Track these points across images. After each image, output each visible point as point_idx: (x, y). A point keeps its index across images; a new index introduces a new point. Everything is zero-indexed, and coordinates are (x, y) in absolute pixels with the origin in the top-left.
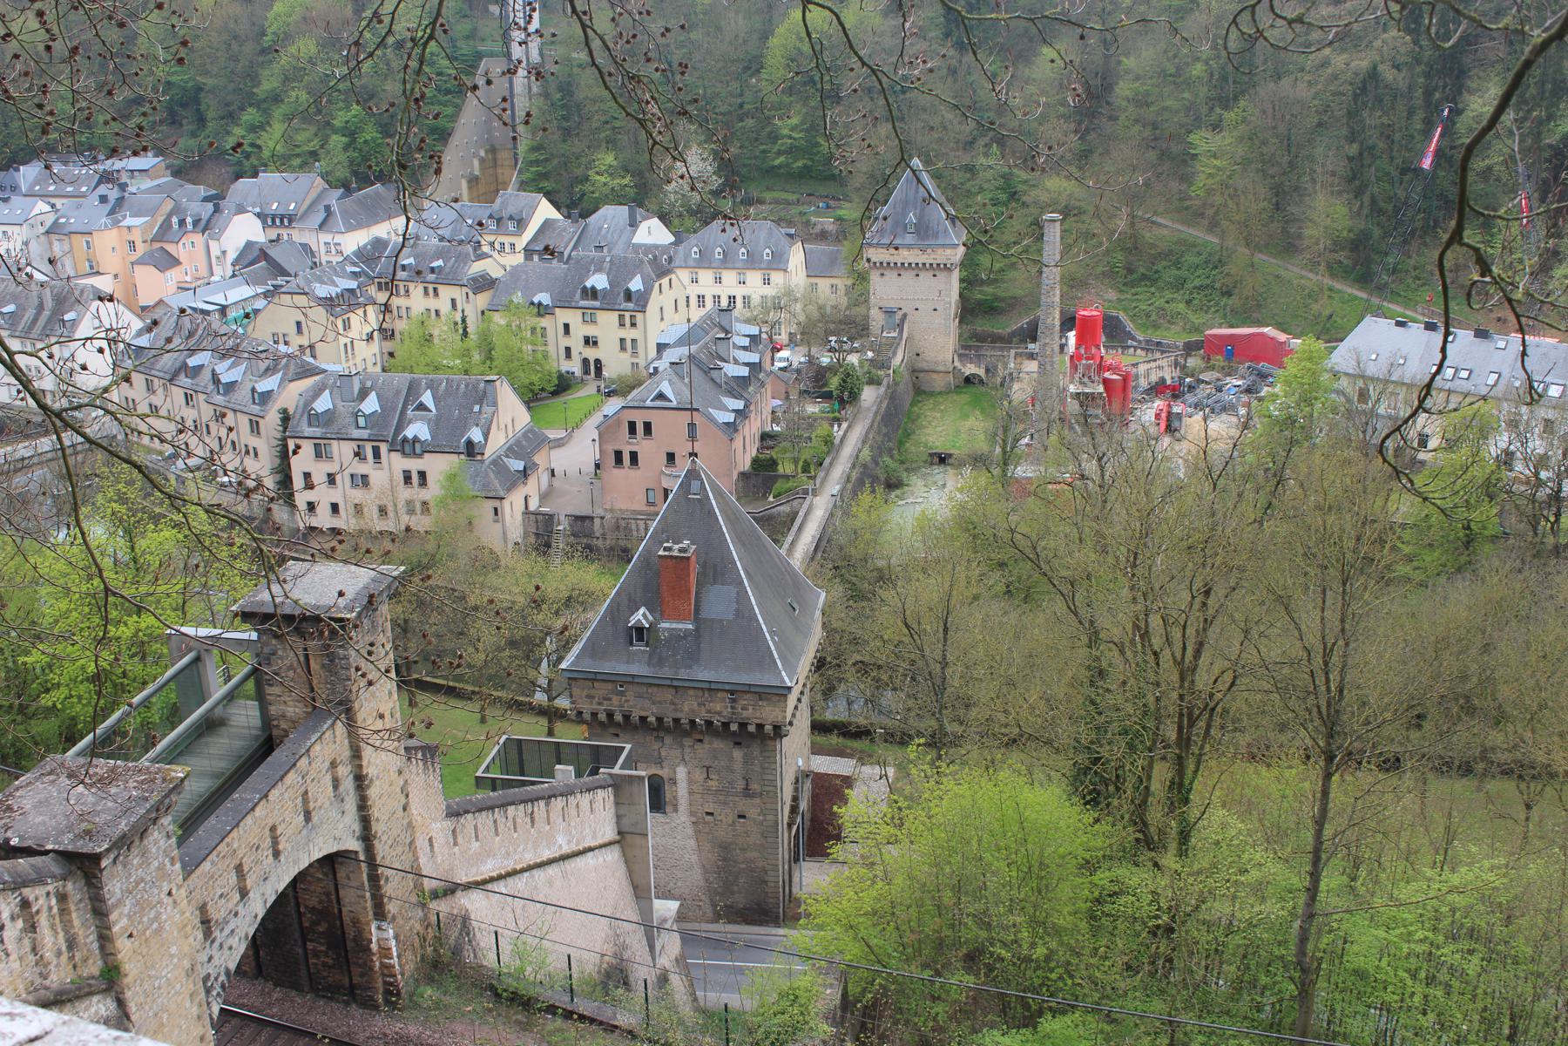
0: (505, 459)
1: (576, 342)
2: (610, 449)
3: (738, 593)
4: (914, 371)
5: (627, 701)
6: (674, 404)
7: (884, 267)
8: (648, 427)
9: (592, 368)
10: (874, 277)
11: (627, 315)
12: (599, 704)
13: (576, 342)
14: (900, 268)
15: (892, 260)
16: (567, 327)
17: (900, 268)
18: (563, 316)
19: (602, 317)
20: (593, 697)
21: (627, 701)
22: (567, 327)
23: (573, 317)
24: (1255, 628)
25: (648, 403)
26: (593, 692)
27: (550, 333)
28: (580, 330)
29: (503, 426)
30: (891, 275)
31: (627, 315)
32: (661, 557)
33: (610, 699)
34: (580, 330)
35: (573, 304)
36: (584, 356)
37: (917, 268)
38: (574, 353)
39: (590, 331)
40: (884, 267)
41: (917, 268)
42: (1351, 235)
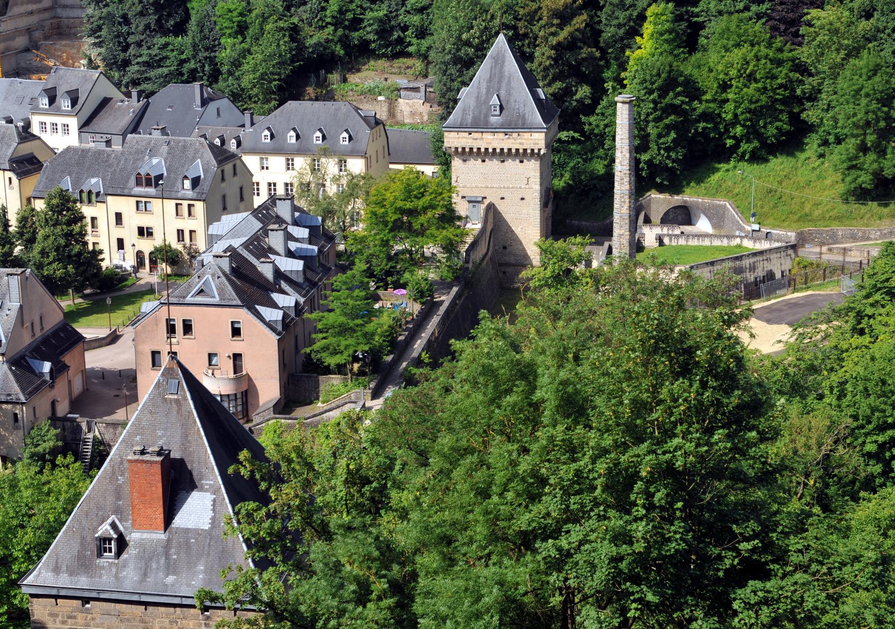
0: (29, 360)
1: (129, 234)
2: (147, 349)
3: (214, 501)
4: (500, 265)
5: (93, 619)
6: (217, 300)
7: (466, 154)
8: (188, 328)
9: (147, 262)
10: (456, 163)
11: (185, 203)
12: (64, 622)
13: (129, 234)
14: (484, 155)
15: (475, 145)
16: (119, 217)
17: (484, 155)
18: (116, 204)
19: (156, 204)
20: (57, 615)
21: (93, 619)
22: (119, 217)
23: (125, 205)
24: (58, 507)
25: (189, 299)
26: (56, 609)
27: (102, 223)
28: (134, 220)
29: (28, 324)
30: (475, 164)
31: (185, 203)
32: (130, 461)
33: (75, 618)
34: (134, 220)
35: (126, 192)
36: (137, 249)
37: (503, 155)
38: (127, 244)
39: (145, 221)
40: (466, 154)
41: (503, 155)
42: (751, 90)
